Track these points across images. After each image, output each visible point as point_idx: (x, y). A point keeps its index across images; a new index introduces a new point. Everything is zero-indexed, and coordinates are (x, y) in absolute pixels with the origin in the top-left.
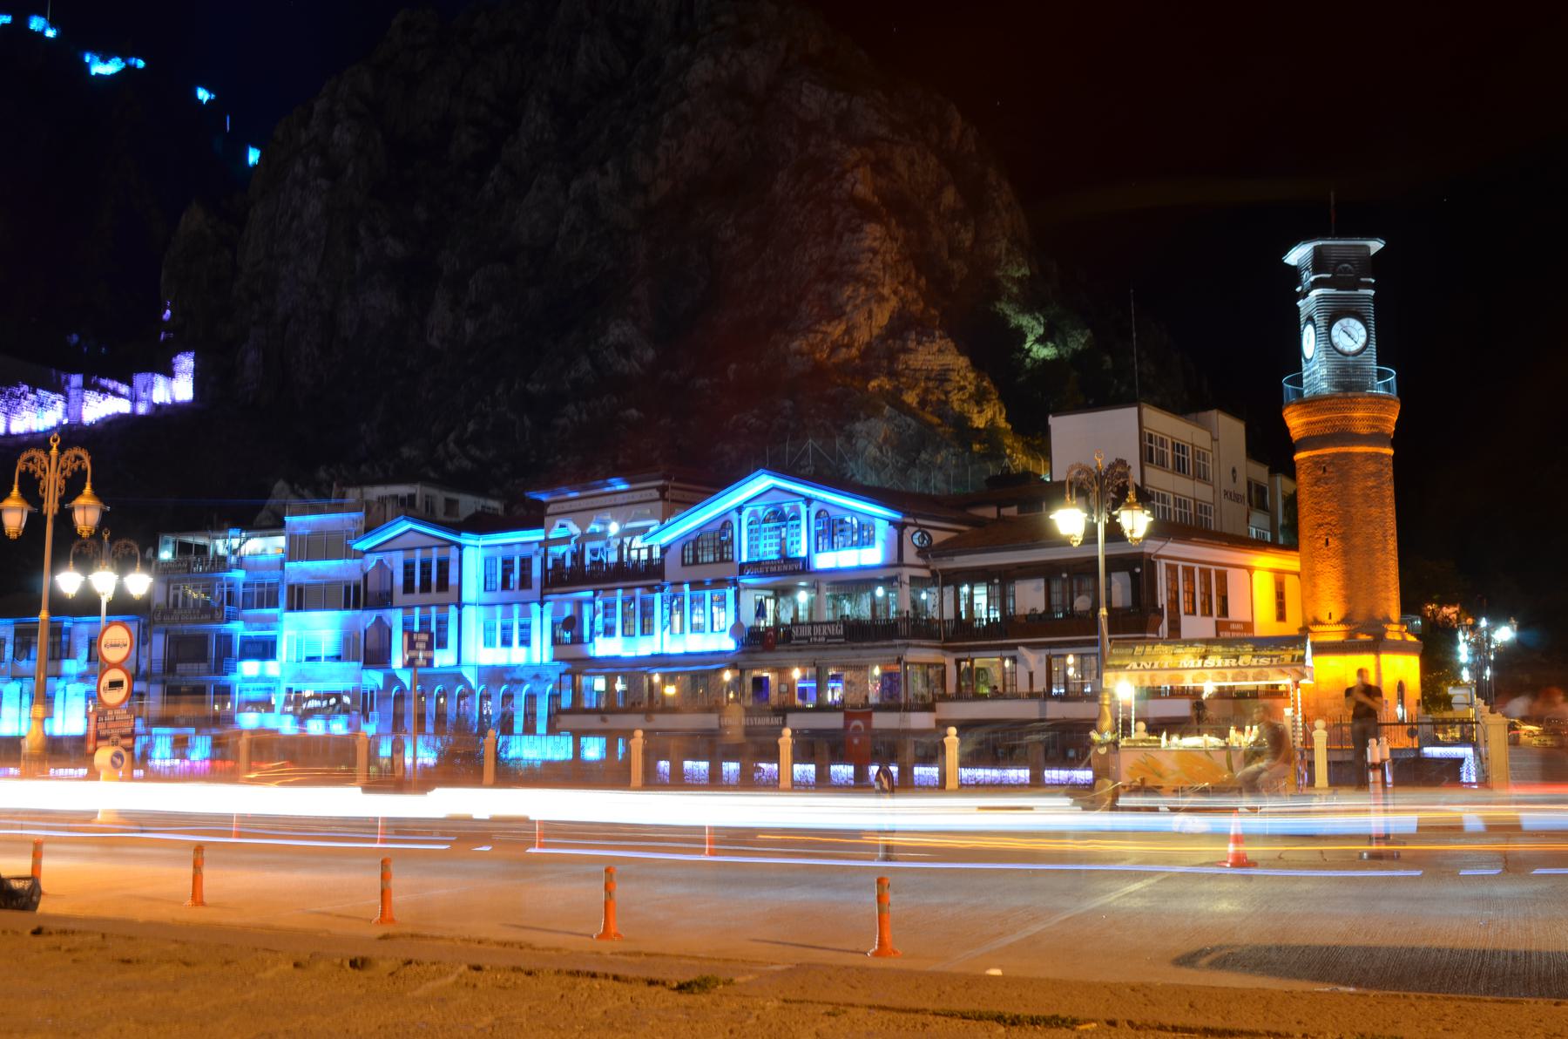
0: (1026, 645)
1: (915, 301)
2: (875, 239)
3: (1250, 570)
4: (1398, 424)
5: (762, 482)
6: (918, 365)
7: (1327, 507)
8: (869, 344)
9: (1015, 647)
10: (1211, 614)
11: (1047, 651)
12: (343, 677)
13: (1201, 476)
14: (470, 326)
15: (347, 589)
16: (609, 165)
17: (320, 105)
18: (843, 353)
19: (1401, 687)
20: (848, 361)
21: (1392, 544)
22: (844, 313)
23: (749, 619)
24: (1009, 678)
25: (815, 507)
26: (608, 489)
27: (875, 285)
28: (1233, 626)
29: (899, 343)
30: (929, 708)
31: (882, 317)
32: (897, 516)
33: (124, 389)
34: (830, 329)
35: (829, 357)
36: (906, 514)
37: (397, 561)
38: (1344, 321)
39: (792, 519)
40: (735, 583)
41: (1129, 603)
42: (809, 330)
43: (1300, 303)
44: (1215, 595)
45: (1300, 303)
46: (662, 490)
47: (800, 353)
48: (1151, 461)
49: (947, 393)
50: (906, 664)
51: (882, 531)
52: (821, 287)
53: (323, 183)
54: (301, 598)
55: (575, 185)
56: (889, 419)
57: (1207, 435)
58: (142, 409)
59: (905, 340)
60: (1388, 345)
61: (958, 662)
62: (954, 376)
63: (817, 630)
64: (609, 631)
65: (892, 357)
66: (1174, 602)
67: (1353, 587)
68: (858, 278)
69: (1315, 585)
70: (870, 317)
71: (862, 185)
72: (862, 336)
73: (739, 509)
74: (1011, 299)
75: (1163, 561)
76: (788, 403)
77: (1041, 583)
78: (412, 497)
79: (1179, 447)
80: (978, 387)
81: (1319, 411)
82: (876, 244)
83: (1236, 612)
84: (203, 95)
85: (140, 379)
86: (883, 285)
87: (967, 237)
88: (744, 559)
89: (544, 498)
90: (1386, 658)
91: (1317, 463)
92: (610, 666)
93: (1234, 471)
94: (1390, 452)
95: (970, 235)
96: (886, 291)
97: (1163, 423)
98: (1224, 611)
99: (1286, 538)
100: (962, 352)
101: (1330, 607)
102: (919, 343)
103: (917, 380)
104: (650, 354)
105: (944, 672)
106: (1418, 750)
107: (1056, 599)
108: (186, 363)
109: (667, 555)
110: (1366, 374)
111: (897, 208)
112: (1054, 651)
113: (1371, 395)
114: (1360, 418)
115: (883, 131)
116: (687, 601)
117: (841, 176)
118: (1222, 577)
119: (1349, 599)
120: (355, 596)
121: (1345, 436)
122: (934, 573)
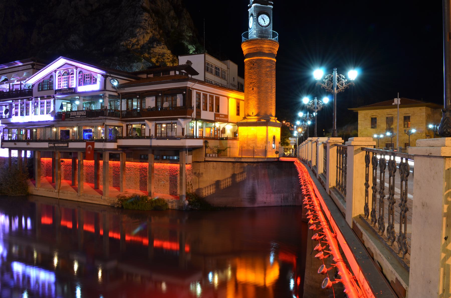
0: (147, 119)
1: (157, 35)
2: (146, 17)
3: (228, 98)
4: (278, 52)
5: (61, 61)
6: (156, 51)
7: (254, 77)
8: (143, 45)
9: (143, 120)
10: (213, 111)
11: (155, 122)
13: (223, 78)
18: (135, 47)
19: (274, 138)
20: (137, 49)
21: (274, 91)
23: (58, 110)
24: (140, 130)
25: (79, 70)
26: (17, 65)
27: (146, 29)
28: (221, 116)
29: (151, 45)
30: (116, 142)
31: (147, 38)
32: (104, 72)
34: (132, 40)
35: (131, 48)
38: (263, 15)
39: (71, 74)
40: (54, 97)
41: (182, 105)
44: (215, 105)
46: (33, 65)
47: (123, 45)
48: (208, 71)
49: (164, 59)
50: (106, 125)
51: (99, 78)
52: (131, 29)
56: (144, 63)
57: (226, 66)
59: (153, 45)
60: (277, 23)
61: (127, 126)
62: (166, 55)
64: (16, 114)
65: (149, 48)
66: (198, 107)
67: (261, 103)
68: (141, 27)
69: (248, 103)
70: (144, 38)
72: (142, 43)
73: (55, 71)
74: (187, 41)
75: (195, 91)
76: (116, 58)
77: (154, 98)
79: (216, 68)
80: (173, 59)
82: (146, 18)
83: (222, 111)
86: (148, 29)
87: (176, 24)
88: (57, 88)
90: (269, 128)
91: (251, 62)
92: (18, 126)
93: (234, 78)
94: (275, 60)
95: (177, 24)
96: (149, 31)
98: (218, 110)
99: (240, 88)
100: (169, 50)
101: (253, 111)
102: (157, 45)
103: (156, 55)
104: (82, 44)
105: (122, 129)
107: (159, 104)
109: (34, 88)
112: (157, 122)
113: (270, 40)
114: (266, 47)
116: (39, 103)
118: (218, 99)
119: (259, 108)
121: (261, 53)
122: (118, 94)
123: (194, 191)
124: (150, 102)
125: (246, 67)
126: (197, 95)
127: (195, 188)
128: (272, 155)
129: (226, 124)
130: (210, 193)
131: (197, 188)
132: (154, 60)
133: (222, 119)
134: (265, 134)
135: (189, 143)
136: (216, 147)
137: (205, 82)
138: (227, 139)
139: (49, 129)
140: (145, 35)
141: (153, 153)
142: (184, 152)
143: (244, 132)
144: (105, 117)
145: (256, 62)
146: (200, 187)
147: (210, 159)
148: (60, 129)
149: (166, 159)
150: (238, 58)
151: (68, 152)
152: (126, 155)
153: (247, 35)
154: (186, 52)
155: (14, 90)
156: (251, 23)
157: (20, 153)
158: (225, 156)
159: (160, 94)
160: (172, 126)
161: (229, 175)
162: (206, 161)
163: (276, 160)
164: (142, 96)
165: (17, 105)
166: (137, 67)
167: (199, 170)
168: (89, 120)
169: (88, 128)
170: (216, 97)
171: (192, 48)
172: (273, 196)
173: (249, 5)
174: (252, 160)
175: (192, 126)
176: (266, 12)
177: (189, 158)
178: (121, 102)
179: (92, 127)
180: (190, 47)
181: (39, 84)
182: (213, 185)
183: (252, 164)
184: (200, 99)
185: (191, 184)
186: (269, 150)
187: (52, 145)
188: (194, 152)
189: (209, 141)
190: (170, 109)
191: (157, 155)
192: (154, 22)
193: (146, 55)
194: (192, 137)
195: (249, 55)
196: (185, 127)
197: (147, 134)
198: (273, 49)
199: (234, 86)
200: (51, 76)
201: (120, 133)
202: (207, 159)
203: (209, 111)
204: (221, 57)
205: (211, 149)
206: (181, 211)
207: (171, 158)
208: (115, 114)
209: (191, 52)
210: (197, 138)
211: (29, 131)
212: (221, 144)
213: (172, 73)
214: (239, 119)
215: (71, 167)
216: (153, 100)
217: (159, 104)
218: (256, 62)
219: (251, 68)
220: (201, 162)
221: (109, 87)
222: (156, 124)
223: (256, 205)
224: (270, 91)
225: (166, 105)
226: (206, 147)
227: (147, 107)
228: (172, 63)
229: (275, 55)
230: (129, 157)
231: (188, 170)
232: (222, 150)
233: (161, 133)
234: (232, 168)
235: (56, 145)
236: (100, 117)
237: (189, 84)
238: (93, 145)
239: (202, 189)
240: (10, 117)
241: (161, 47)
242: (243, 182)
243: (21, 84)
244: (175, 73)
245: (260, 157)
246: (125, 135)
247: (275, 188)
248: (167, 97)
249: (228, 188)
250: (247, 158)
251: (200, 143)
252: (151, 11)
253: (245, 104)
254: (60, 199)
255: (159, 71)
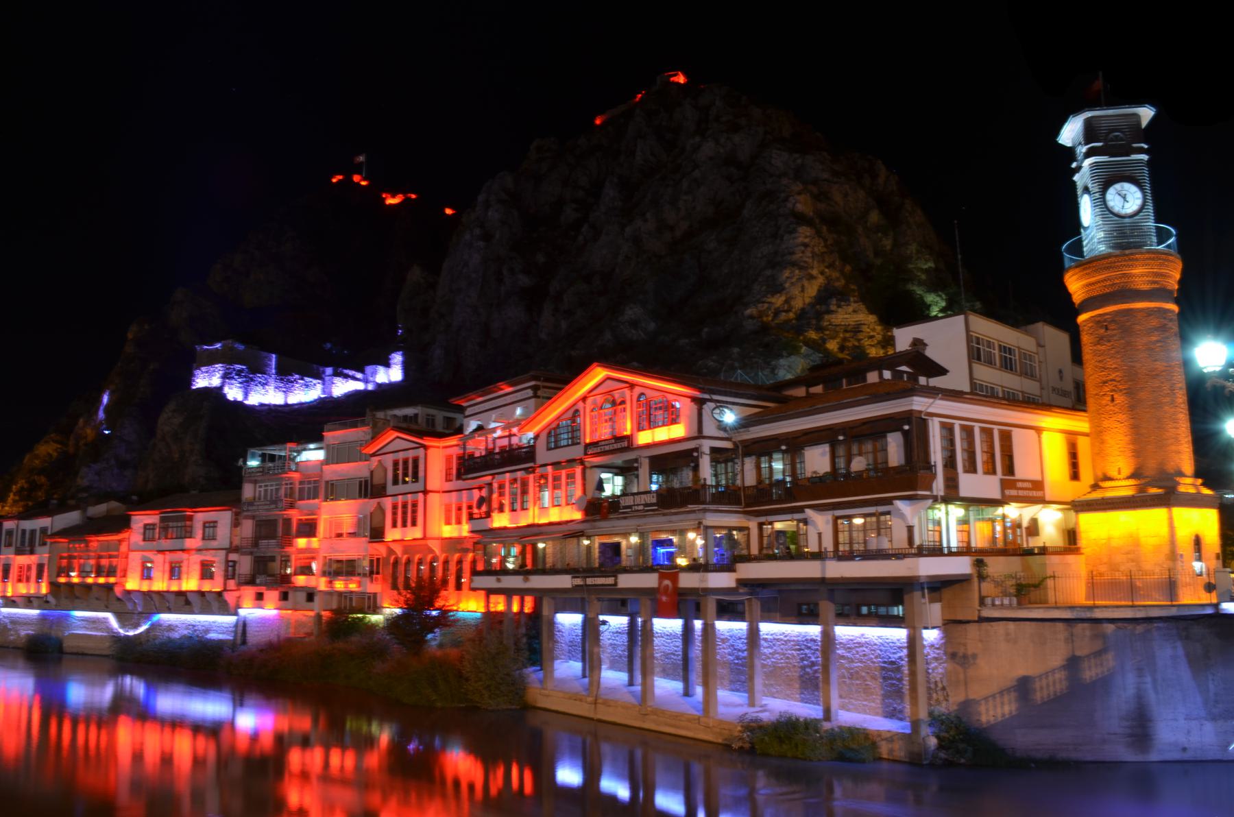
1: (838, 279)
4: (1180, 282)
5: (599, 374)
7: (1111, 363)
8: (803, 309)
9: (801, 510)
10: (994, 472)
12: (358, 549)
13: (1028, 373)
14: (564, 325)
15: (360, 482)
16: (648, 215)
17: (481, 198)
18: (783, 316)
19: (1198, 542)
20: (788, 321)
22: (784, 289)
24: (795, 537)
28: (1020, 485)
29: (824, 308)
30: (730, 569)
31: (812, 290)
33: (359, 375)
34: (773, 300)
36: (702, 390)
37: (388, 461)
38: (1118, 186)
41: (903, 462)
42: (759, 301)
43: (1076, 178)
45: (1076, 178)
46: (535, 388)
47: (751, 317)
48: (979, 359)
49: (859, 340)
50: (707, 528)
52: (768, 272)
53: (481, 244)
54: (333, 491)
55: (628, 230)
56: (806, 356)
58: (370, 387)
60: (1164, 203)
61: (761, 525)
62: (865, 328)
63: (638, 499)
65: (819, 316)
66: (950, 463)
68: (794, 264)
69: (1103, 442)
70: (803, 291)
71: (802, 204)
72: (798, 304)
74: (921, 283)
75: (937, 420)
76: (736, 350)
77: (826, 448)
78: (416, 415)
79: (1003, 349)
80: (884, 336)
81: (1098, 270)
82: (807, 240)
83: (1024, 470)
84: (448, 211)
85: (369, 369)
86: (812, 268)
87: (887, 243)
88: (588, 441)
89: (465, 404)
90: (1178, 512)
91: (1099, 322)
93: (1060, 372)
94: (1174, 307)
96: (814, 272)
97: (987, 328)
98: (1009, 469)
99: (1075, 401)
100: (871, 313)
101: (1120, 464)
102: (839, 306)
104: (652, 326)
105: (749, 535)
106: (1216, 606)
108: (397, 358)
110: (1144, 234)
111: (831, 222)
113: (1149, 252)
114: (1139, 274)
115: (825, 175)
116: (550, 480)
117: (786, 200)
118: (1006, 438)
120: (370, 489)
121: (1126, 293)
122: (735, 443)
123: (953, 708)
124: (817, 460)
125: (1085, 338)
126: (945, 433)
127: (956, 697)
128: (1192, 597)
129: (1039, 506)
130: (1003, 715)
131: (961, 698)
132: (832, 346)
133: (1025, 493)
134: (1164, 530)
135: (928, 567)
136: (1011, 577)
137: (980, 393)
138: (1044, 551)
139: (575, 540)
140: (806, 283)
141: (832, 600)
142: (917, 594)
143: (1099, 528)
144: (702, 507)
145: (1113, 321)
146: (971, 697)
147: (996, 614)
148: (597, 541)
149: (870, 615)
150: (1063, 313)
151: (616, 600)
152: (762, 606)
153: (1077, 248)
154: (919, 314)
155: (497, 450)
156: (1087, 211)
157: (509, 604)
158: (1043, 602)
159: (841, 438)
160: (878, 522)
161: (1056, 658)
162: (982, 620)
163: (1210, 611)
164: (794, 445)
165: (501, 487)
166: (790, 367)
167: (965, 645)
168: (664, 515)
169: (664, 536)
170: (1001, 432)
171: (936, 303)
172: (1209, 727)
173: (1074, 165)
174: (1129, 614)
175: (936, 517)
176: (1127, 174)
177: (935, 611)
178: (743, 464)
179: (673, 532)
180: (930, 298)
181: (550, 433)
182: (1008, 690)
183: (1130, 627)
184: (952, 442)
185: (944, 689)
186: (1182, 579)
187: (579, 582)
188: (947, 593)
189: (987, 560)
190: (872, 474)
191: (843, 605)
192: (826, 246)
193: (813, 335)
194: (937, 551)
195: (1088, 304)
196: (914, 522)
197: (812, 547)
198: (1162, 275)
199: (1064, 394)
200: (574, 413)
201: (744, 545)
202: (986, 613)
203: (985, 473)
204: (1016, 317)
205: (997, 584)
206: (916, 762)
207: (882, 610)
208: (730, 497)
209: (934, 311)
210: (951, 554)
211: (529, 549)
212: (1026, 568)
213: (872, 377)
214: (1080, 490)
215: (625, 638)
216: (823, 454)
217: (841, 463)
218: (1113, 321)
219: (1100, 340)
220: (968, 622)
221: (709, 429)
222: (836, 518)
223: (1154, 757)
224: (1168, 399)
225: (859, 464)
226: (982, 577)
227: (809, 475)
228: (884, 347)
229: (1171, 292)
230: (769, 611)
231: (932, 646)
232: (1029, 586)
233: (851, 543)
234: (1066, 640)
235: (590, 581)
236: (691, 507)
237: (919, 404)
238: (674, 578)
239: (977, 702)
240: (488, 515)
241: (850, 309)
242: (1104, 685)
243: (510, 436)
244: (881, 376)
245: (1155, 604)
246: (755, 550)
247: (1216, 702)
248: (860, 443)
249: (1058, 701)
250: (1113, 607)
251: (962, 566)
252: (817, 221)
253: (1093, 445)
254: (600, 721)
255: (840, 374)
